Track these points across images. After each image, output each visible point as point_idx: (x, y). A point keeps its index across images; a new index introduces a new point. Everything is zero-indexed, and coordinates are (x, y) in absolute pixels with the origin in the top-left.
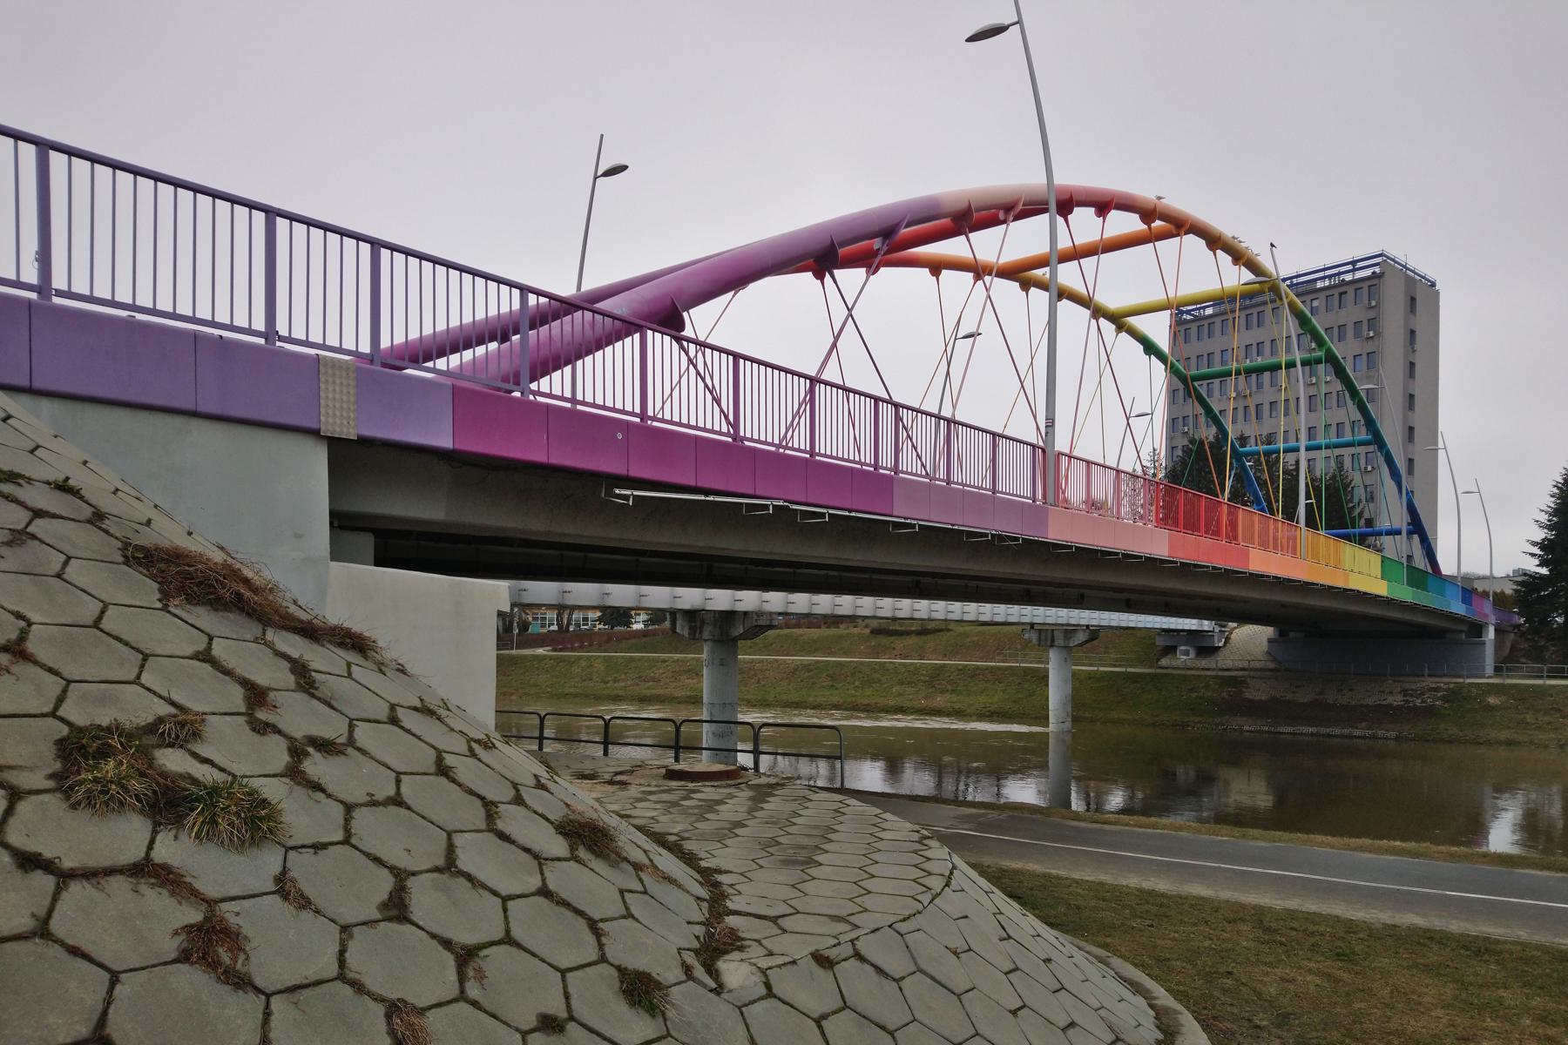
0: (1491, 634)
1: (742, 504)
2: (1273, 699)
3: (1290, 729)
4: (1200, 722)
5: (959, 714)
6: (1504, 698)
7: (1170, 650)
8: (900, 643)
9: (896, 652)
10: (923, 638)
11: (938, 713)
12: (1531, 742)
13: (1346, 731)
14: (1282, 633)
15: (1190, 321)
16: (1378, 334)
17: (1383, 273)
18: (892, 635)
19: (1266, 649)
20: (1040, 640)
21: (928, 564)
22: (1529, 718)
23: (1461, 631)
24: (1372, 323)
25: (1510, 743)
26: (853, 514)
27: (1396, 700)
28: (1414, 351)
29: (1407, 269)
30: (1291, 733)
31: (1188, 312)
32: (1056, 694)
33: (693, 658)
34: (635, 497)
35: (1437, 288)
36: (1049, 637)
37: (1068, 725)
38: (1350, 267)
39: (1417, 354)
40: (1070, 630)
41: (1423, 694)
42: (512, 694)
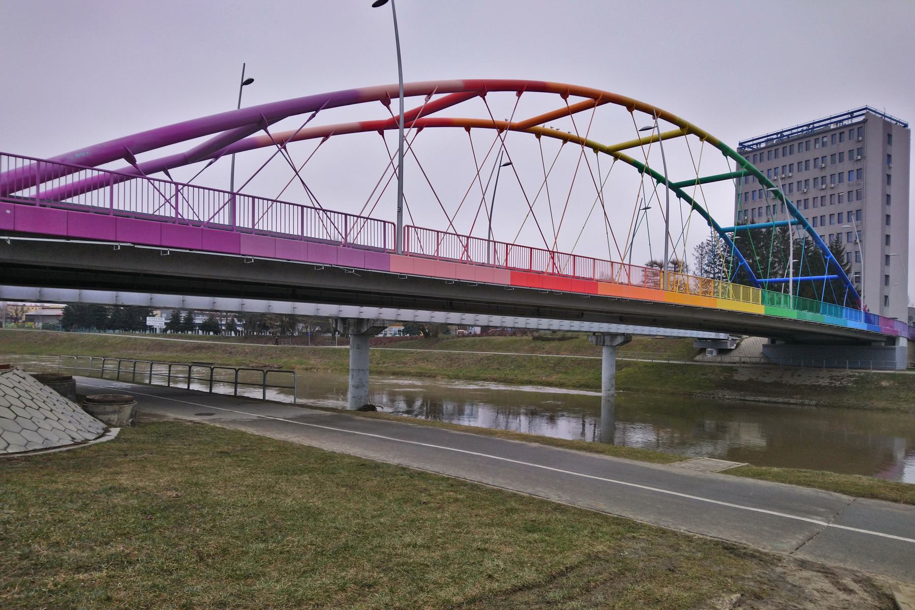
0: (903, 342)
1: (113, 245)
2: (750, 380)
3: (752, 398)
4: (700, 393)
5: (561, 385)
6: (892, 382)
7: (702, 351)
8: (548, 345)
9: (545, 351)
10: (563, 342)
11: (550, 384)
12: (898, 409)
13: (786, 400)
14: (773, 342)
15: (750, 152)
16: (864, 158)
17: (867, 120)
18: (544, 341)
19: (762, 351)
20: (597, 341)
21: (302, 282)
22: (902, 395)
23: (882, 341)
24: (860, 151)
25: (885, 410)
26: (194, 252)
27: (824, 382)
28: (890, 168)
29: (885, 116)
30: (752, 401)
31: (749, 146)
32: (606, 372)
33: (428, 352)
34: (11, 240)
35: (909, 128)
36: (602, 340)
37: (612, 392)
38: (849, 116)
39: (893, 169)
40: (614, 336)
41: (843, 379)
42: (328, 369)
